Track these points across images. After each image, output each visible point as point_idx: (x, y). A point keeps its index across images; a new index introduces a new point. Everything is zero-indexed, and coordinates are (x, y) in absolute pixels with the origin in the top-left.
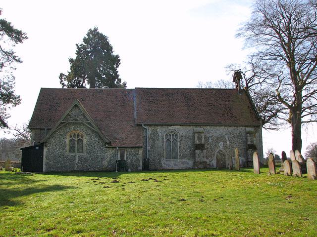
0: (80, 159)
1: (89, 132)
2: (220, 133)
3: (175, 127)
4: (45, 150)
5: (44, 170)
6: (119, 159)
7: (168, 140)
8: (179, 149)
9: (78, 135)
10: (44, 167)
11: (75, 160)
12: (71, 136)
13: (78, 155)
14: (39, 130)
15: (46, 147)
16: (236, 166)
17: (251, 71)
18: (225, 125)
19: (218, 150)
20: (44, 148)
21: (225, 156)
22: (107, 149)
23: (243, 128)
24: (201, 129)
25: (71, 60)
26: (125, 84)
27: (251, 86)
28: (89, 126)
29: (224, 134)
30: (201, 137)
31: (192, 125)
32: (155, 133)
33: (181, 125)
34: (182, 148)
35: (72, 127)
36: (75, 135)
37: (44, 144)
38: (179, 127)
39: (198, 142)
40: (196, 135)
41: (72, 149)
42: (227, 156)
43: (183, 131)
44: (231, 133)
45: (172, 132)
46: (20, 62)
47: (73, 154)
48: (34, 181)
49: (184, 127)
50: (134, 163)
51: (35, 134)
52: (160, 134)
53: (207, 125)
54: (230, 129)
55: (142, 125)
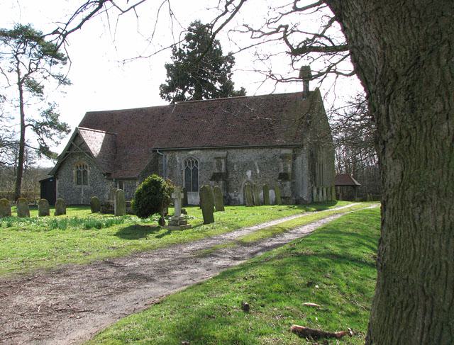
3: (194, 151)
4: (57, 182)
7: (187, 169)
9: (193, 162)
13: (83, 187)
16: (271, 203)
18: (254, 147)
19: (245, 181)
25: (168, 67)
26: (242, 92)
29: (253, 159)
30: (221, 164)
32: (173, 161)
33: (201, 149)
38: (199, 151)
39: (217, 171)
41: (79, 183)
43: (203, 156)
44: (262, 157)
46: (69, 83)
47: (79, 186)
52: (178, 161)
53: (232, 148)
54: (261, 152)
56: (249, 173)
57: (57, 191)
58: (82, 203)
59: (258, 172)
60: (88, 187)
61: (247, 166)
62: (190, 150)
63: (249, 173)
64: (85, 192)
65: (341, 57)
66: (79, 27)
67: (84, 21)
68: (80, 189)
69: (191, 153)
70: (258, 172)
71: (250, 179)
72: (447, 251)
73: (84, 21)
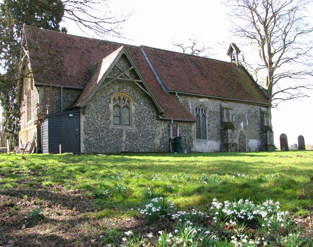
0: (128, 135)
1: (138, 96)
2: (241, 111)
4: (83, 119)
5: (82, 150)
6: (172, 138)
8: (207, 127)
10: (82, 145)
11: (121, 136)
12: (115, 100)
13: (125, 128)
14: (51, 89)
15: (84, 114)
17: (190, 48)
20: (82, 115)
21: (245, 138)
22: (159, 122)
23: (258, 107)
24: (226, 104)
27: (238, 61)
28: (141, 88)
29: (244, 113)
30: (229, 115)
31: (219, 99)
34: (210, 126)
35: (117, 87)
36: (119, 99)
37: (81, 110)
38: (207, 100)
40: (225, 111)
42: (247, 138)
45: (201, 106)
48: (254, 168)
49: (212, 101)
50: (187, 142)
51: (45, 95)
54: (249, 107)
55: (175, 93)
56: (242, 124)
57: (82, 131)
58: (123, 150)
59: (247, 124)
60: (133, 129)
61: (240, 118)
62: (201, 97)
63: (242, 124)
64: (128, 135)
65: (268, 18)
66: (85, 26)
67: (85, 21)
68: (122, 131)
69: (201, 100)
70: (247, 124)
71: (243, 130)
72: (28, 102)
73: (85, 21)
